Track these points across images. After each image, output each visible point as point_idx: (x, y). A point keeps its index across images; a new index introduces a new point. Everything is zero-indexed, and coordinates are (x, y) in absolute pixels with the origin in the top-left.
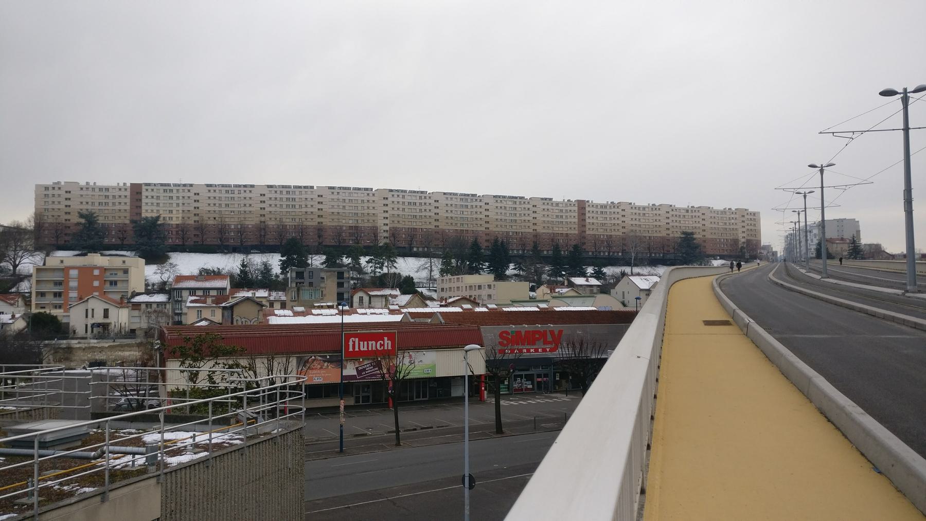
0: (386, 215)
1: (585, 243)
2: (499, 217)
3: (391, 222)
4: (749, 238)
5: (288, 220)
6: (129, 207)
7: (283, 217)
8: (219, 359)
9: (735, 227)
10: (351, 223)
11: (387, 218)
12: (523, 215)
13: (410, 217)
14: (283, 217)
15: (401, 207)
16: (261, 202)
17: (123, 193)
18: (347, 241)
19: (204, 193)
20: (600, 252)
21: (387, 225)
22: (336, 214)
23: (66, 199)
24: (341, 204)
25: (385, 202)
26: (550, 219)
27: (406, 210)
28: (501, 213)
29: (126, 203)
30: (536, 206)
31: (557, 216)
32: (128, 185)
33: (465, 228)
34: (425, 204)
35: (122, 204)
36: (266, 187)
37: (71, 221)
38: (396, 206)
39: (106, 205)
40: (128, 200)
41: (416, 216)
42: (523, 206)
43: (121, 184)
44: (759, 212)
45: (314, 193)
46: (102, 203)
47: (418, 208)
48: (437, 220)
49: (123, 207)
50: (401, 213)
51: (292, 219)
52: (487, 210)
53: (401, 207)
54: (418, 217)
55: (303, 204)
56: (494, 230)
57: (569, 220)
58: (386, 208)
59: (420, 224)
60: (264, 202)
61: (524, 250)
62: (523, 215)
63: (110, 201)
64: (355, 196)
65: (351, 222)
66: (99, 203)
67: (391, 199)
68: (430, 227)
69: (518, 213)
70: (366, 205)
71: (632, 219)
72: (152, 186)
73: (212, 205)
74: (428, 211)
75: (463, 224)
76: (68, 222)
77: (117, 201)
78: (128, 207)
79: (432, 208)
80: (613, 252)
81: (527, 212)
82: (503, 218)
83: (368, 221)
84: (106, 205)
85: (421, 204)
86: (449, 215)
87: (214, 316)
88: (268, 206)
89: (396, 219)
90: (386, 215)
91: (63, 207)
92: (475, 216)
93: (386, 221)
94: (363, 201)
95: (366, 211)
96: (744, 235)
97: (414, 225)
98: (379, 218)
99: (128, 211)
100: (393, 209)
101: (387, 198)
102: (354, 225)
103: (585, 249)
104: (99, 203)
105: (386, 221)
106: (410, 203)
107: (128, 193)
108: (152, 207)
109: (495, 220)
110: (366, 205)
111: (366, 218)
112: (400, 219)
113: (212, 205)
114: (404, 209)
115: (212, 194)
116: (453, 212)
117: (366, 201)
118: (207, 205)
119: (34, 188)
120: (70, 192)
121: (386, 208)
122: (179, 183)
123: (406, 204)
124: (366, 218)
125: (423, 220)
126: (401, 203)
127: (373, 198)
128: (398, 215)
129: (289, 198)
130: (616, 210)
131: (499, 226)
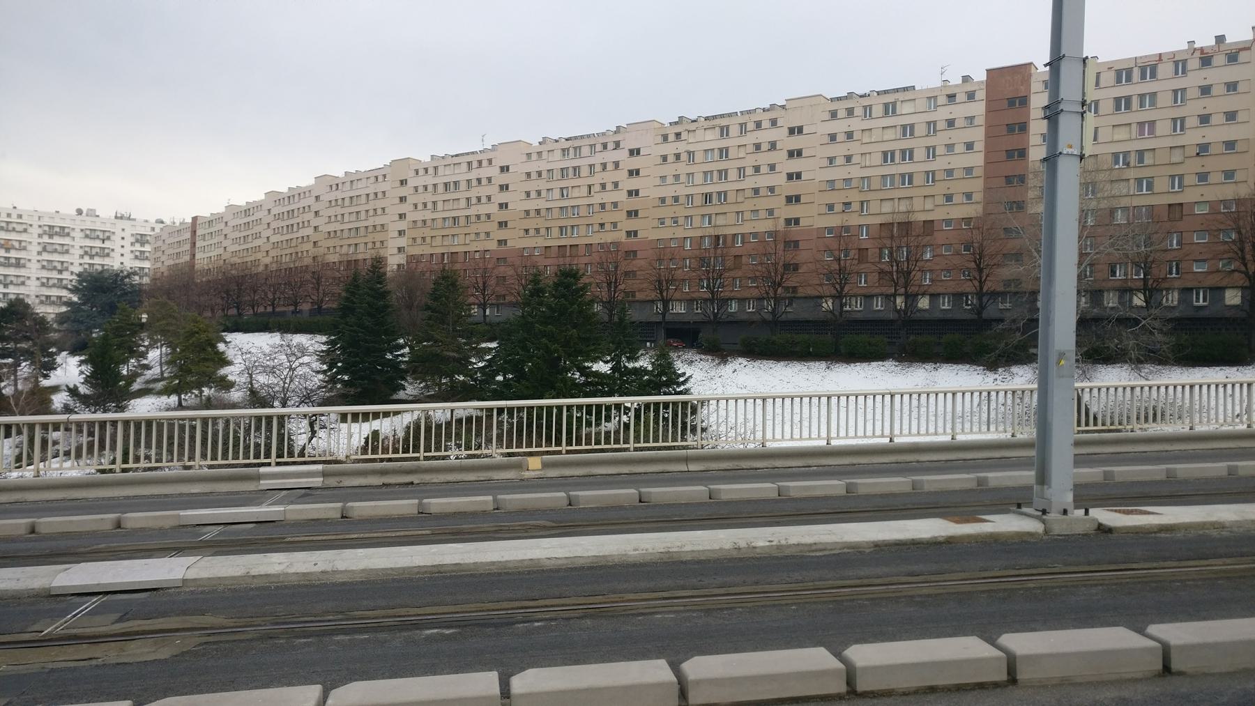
1: (796, 267)
2: (668, 192)
4: (416, 251)
5: (1121, 189)
6: (982, 155)
7: (1101, 176)
9: (379, 220)
12: (749, 171)
14: (870, 196)
17: (959, 111)
20: (725, 301)
23: (791, 154)
26: (855, 172)
28: (677, 177)
29: (969, 146)
30: (800, 130)
31: (887, 156)
32: (980, 76)
35: (1217, 119)
37: (509, 244)
39: (904, 159)
40: (978, 135)
42: (751, 139)
43: (956, 80)
46: (893, 153)
47: (1162, 116)
49: (960, 161)
51: (1139, 181)
57: (939, 164)
59: (929, 206)
61: (839, 296)
62: (749, 171)
63: (918, 145)
66: (885, 154)
69: (732, 166)
71: (528, 194)
74: (764, 169)
77: (940, 140)
78: (977, 159)
80: (1186, 291)
81: (764, 159)
82: (682, 191)
84: (904, 159)
92: (597, 199)
96: (403, 242)
99: (979, 172)
103: (795, 289)
104: (885, 154)
107: (978, 109)
125: (940, 189)
129: (1128, 100)
130: (610, 156)
131: (668, 222)
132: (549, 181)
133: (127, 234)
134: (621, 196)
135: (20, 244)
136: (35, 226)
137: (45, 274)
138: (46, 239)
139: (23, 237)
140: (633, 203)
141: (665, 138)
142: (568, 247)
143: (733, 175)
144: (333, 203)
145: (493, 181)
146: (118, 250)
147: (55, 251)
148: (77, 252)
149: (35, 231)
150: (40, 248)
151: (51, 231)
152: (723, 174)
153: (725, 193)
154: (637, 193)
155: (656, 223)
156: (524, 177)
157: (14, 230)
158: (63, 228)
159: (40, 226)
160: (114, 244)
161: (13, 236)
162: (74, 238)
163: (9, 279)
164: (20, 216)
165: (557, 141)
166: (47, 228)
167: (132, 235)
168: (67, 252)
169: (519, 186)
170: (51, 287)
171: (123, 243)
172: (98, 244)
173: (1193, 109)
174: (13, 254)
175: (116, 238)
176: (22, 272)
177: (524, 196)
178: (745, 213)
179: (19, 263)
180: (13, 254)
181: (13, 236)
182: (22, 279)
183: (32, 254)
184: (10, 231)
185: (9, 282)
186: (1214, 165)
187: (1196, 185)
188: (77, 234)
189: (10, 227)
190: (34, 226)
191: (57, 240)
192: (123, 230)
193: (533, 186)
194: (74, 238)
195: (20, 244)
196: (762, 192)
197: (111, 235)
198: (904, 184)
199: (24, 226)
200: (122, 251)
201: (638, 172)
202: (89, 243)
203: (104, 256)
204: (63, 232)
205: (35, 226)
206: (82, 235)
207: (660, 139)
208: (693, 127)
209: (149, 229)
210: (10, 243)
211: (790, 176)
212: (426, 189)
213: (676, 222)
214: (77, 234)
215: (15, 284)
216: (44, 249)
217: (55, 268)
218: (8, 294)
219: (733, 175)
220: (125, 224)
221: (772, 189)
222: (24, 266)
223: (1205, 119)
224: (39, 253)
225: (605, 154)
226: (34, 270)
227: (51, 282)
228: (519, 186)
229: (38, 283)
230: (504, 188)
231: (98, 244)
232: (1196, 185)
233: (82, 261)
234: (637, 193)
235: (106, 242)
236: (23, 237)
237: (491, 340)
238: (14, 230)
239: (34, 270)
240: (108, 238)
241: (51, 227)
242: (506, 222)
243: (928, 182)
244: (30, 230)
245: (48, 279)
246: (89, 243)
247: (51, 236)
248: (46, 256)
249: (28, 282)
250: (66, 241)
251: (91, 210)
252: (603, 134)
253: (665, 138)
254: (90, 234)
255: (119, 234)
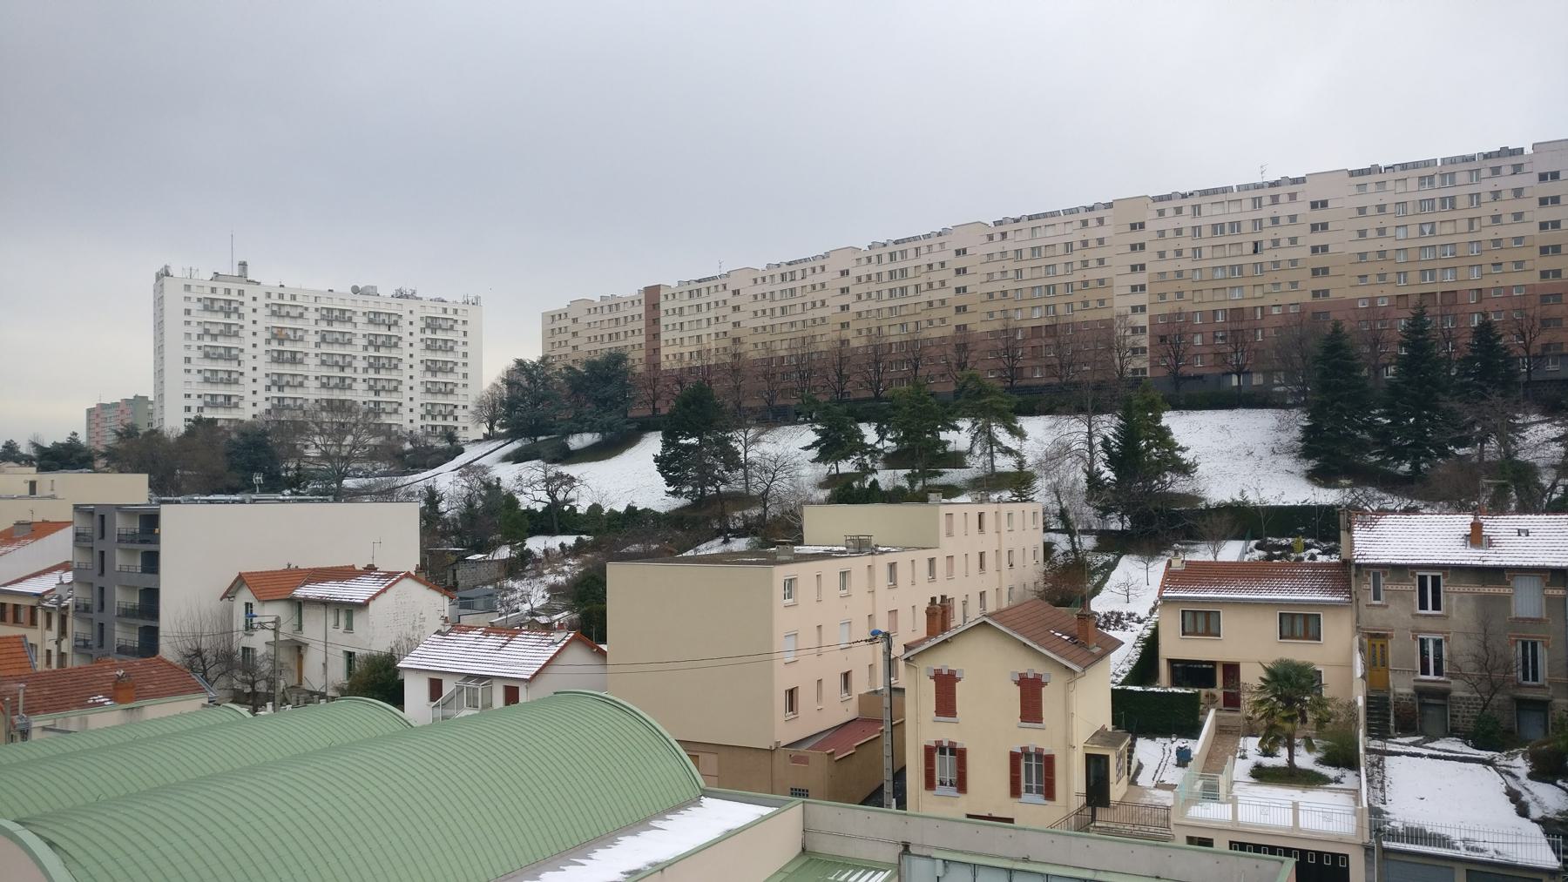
0: (1139, 278)
2: (995, 287)
3: (1156, 298)
8: (1390, 742)
10: (1038, 317)
11: (1143, 288)
13: (1219, 274)
15: (1187, 244)
16: (1133, 247)
18: (1027, 373)
19: (1344, 200)
21: (1143, 309)
22: (1173, 276)
23: (1314, 228)
24: (1010, 266)
25: (1137, 237)
27: (1206, 253)
33: (1446, 282)
34: (1275, 220)
36: (1347, 174)
38: (1170, 246)
41: (1240, 266)
44: (1540, 198)
45: (1526, 168)
48: (961, 309)
50: (1185, 265)
52: (961, 271)
53: (1187, 244)
54: (1247, 271)
55: (923, 280)
56: (1351, 294)
58: (1137, 258)
59: (1258, 293)
60: (1142, 246)
64: (1047, 236)
65: (1037, 314)
67: (1153, 226)
68: (1294, 298)
70: (1077, 257)
72: (1176, 198)
73: (1371, 234)
75: (1432, 271)
76: (1321, 299)
79: (1301, 231)
83: (931, 322)
85: (1258, 224)
86: (1371, 246)
87: (1436, 606)
88: (1156, 257)
89: (1170, 288)
90: (1139, 278)
91: (1307, 253)
93: (1140, 299)
94: (1069, 246)
95: (1077, 277)
97: (1236, 299)
98: (1117, 292)
100: (1162, 255)
101: (1142, 225)
102: (1044, 322)
105: (1140, 299)
106: (1217, 229)
108: (1180, 261)
109: (752, 331)
110: (1077, 257)
111: (1077, 297)
112: (1185, 286)
113: (1371, 234)
114: (1197, 252)
115: (1371, 200)
116: (1389, 232)
117: (1077, 246)
118: (1355, 236)
119: (1537, 176)
120: (1324, 204)
121: (1137, 258)
122: (1258, 180)
123: (1207, 232)
124: (1077, 297)
125: (1268, 279)
126: (1187, 232)
127: (1100, 232)
128: (1179, 273)
132: (773, 300)
133: (415, 318)
134: (948, 294)
135: (295, 333)
136: (312, 310)
137: (325, 371)
138: (323, 326)
139: (299, 324)
140: (962, 300)
141: (991, 237)
142: (1044, 328)
143: (911, 291)
144: (592, 339)
145: (728, 303)
146: (407, 339)
147: (336, 342)
148: (360, 342)
149: (312, 316)
150: (317, 338)
151: (329, 316)
152: (903, 290)
153: (1054, 286)
154: (965, 289)
155: (985, 317)
156: (752, 299)
157: (288, 314)
158: (343, 311)
159: (317, 310)
160: (403, 331)
161: (287, 323)
162: (356, 324)
163: (286, 379)
164: (294, 297)
165: (885, 245)
166: (324, 312)
167: (422, 318)
168: (350, 342)
169: (748, 307)
170: (332, 388)
171: (411, 329)
172: (383, 331)
173: (1488, 209)
174: (288, 346)
175: (404, 323)
176: (299, 370)
177: (752, 315)
178: (1409, 275)
179: (295, 358)
180: (288, 346)
181: (287, 323)
182: (300, 379)
183: (309, 346)
184: (283, 316)
185: (284, 383)
186: (1371, 269)
187: (1358, 286)
188: (360, 319)
189: (284, 311)
190: (310, 310)
191: (337, 327)
192: (411, 312)
193: (759, 306)
194: (356, 324)
195: (295, 333)
196: (1091, 284)
197: (173, 290)
198: (1049, 293)
199: (300, 310)
200: (411, 340)
201: (965, 270)
202: (373, 330)
203: (391, 347)
204: (344, 316)
205: (312, 310)
206: (365, 320)
207: (985, 239)
208: (1017, 226)
209: (441, 311)
210: (284, 332)
211: (958, 290)
212: (814, 271)
213: (991, 316)
214: (360, 319)
215: (291, 386)
216: (324, 339)
217: (337, 364)
218: (283, 398)
219: (911, 291)
220: (408, 305)
221: (943, 302)
222: (301, 362)
223: (1496, 219)
224: (317, 345)
225: (870, 266)
226: (312, 367)
227: (332, 382)
228: (748, 307)
229: (317, 384)
230: (736, 309)
231: (383, 331)
232: (1358, 286)
233: (366, 354)
234: (965, 289)
235: (392, 328)
236: (299, 324)
237: (1302, 526)
238: (288, 314)
239: (312, 367)
240: (396, 323)
241: (330, 310)
242: (739, 322)
243: (1257, 273)
244: (306, 315)
245: (328, 378)
246: (373, 330)
247: (330, 322)
248: (325, 349)
249: (306, 383)
250: (347, 328)
251: (372, 287)
252: (929, 236)
253: (991, 237)
254: (374, 318)
255: (407, 317)
